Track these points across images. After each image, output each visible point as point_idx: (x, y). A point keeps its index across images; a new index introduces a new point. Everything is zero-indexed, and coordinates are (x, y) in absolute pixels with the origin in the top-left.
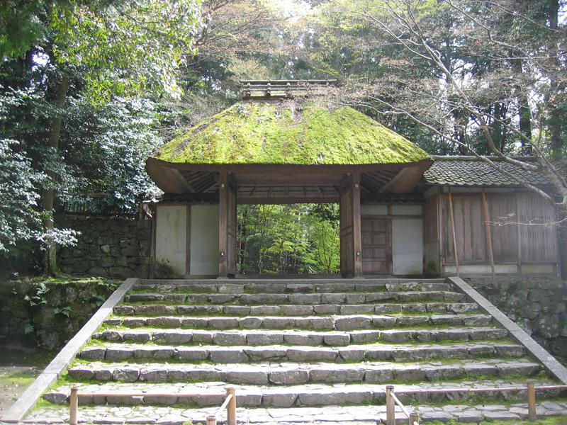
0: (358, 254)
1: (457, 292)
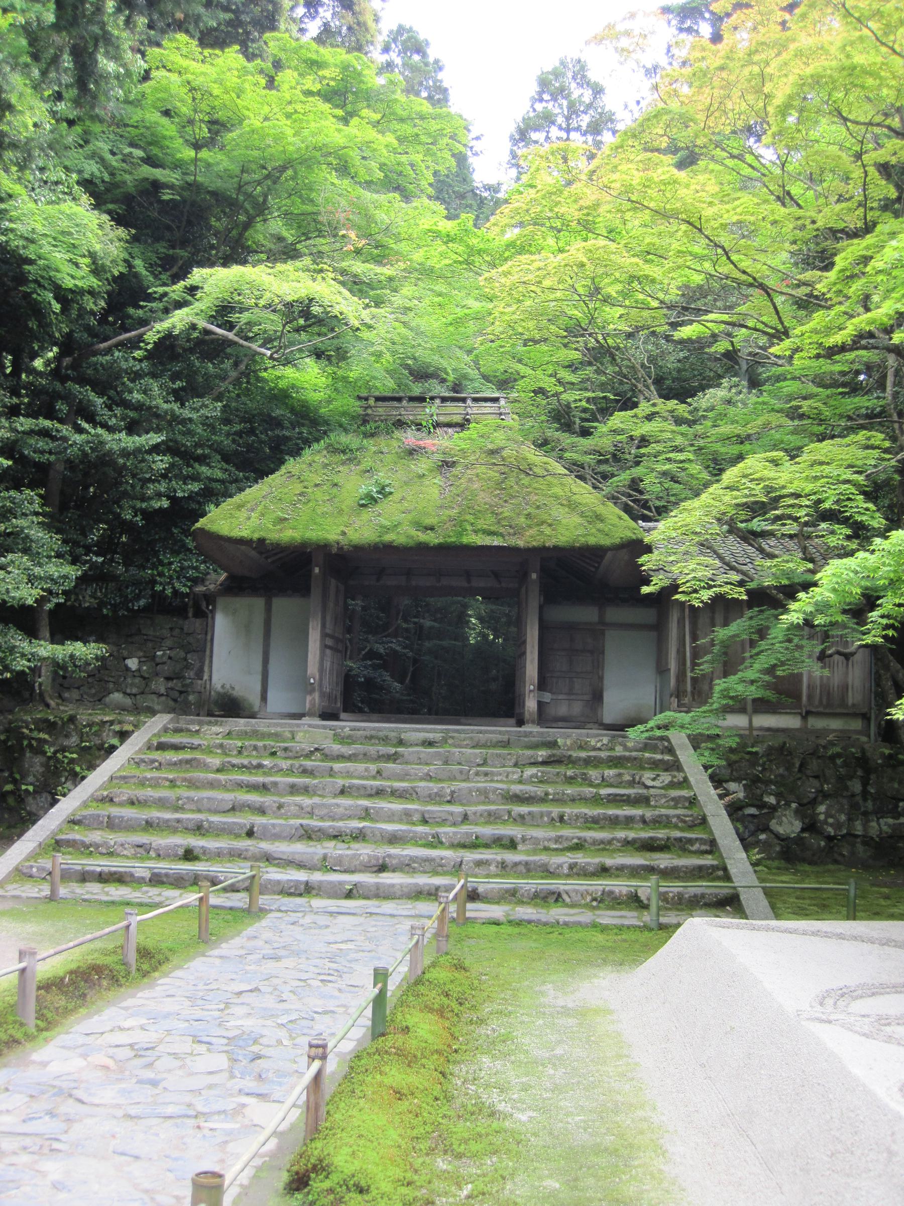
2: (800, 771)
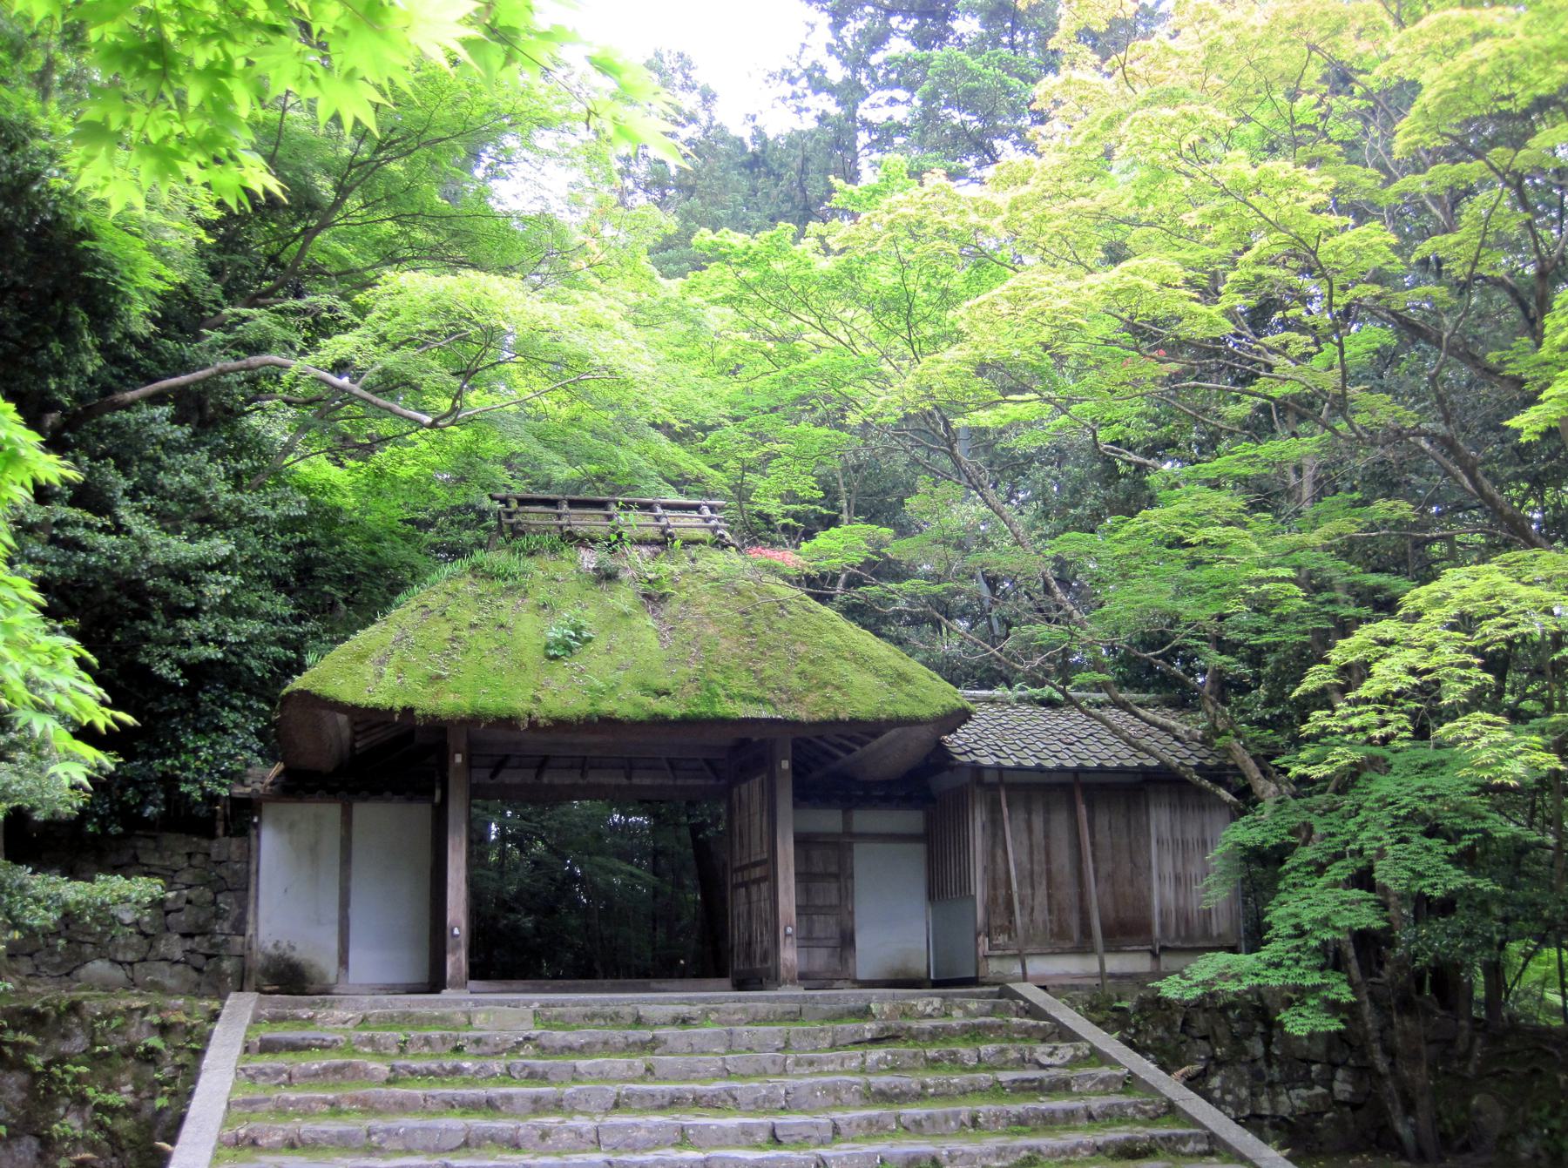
0: (789, 930)
1: (1034, 1018)
2: (1183, 1031)
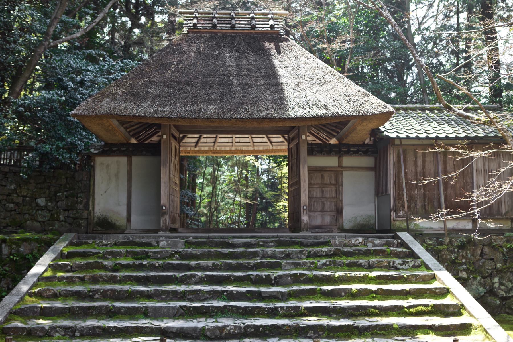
0: (305, 207)
